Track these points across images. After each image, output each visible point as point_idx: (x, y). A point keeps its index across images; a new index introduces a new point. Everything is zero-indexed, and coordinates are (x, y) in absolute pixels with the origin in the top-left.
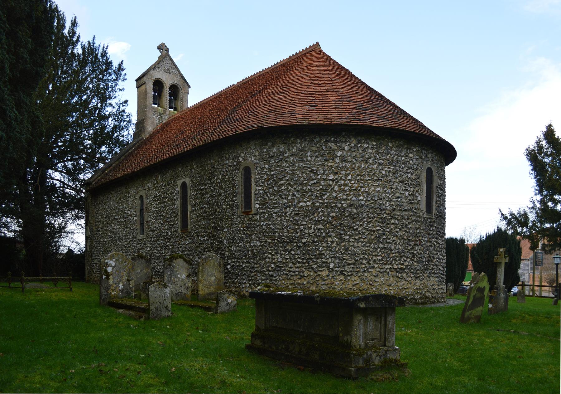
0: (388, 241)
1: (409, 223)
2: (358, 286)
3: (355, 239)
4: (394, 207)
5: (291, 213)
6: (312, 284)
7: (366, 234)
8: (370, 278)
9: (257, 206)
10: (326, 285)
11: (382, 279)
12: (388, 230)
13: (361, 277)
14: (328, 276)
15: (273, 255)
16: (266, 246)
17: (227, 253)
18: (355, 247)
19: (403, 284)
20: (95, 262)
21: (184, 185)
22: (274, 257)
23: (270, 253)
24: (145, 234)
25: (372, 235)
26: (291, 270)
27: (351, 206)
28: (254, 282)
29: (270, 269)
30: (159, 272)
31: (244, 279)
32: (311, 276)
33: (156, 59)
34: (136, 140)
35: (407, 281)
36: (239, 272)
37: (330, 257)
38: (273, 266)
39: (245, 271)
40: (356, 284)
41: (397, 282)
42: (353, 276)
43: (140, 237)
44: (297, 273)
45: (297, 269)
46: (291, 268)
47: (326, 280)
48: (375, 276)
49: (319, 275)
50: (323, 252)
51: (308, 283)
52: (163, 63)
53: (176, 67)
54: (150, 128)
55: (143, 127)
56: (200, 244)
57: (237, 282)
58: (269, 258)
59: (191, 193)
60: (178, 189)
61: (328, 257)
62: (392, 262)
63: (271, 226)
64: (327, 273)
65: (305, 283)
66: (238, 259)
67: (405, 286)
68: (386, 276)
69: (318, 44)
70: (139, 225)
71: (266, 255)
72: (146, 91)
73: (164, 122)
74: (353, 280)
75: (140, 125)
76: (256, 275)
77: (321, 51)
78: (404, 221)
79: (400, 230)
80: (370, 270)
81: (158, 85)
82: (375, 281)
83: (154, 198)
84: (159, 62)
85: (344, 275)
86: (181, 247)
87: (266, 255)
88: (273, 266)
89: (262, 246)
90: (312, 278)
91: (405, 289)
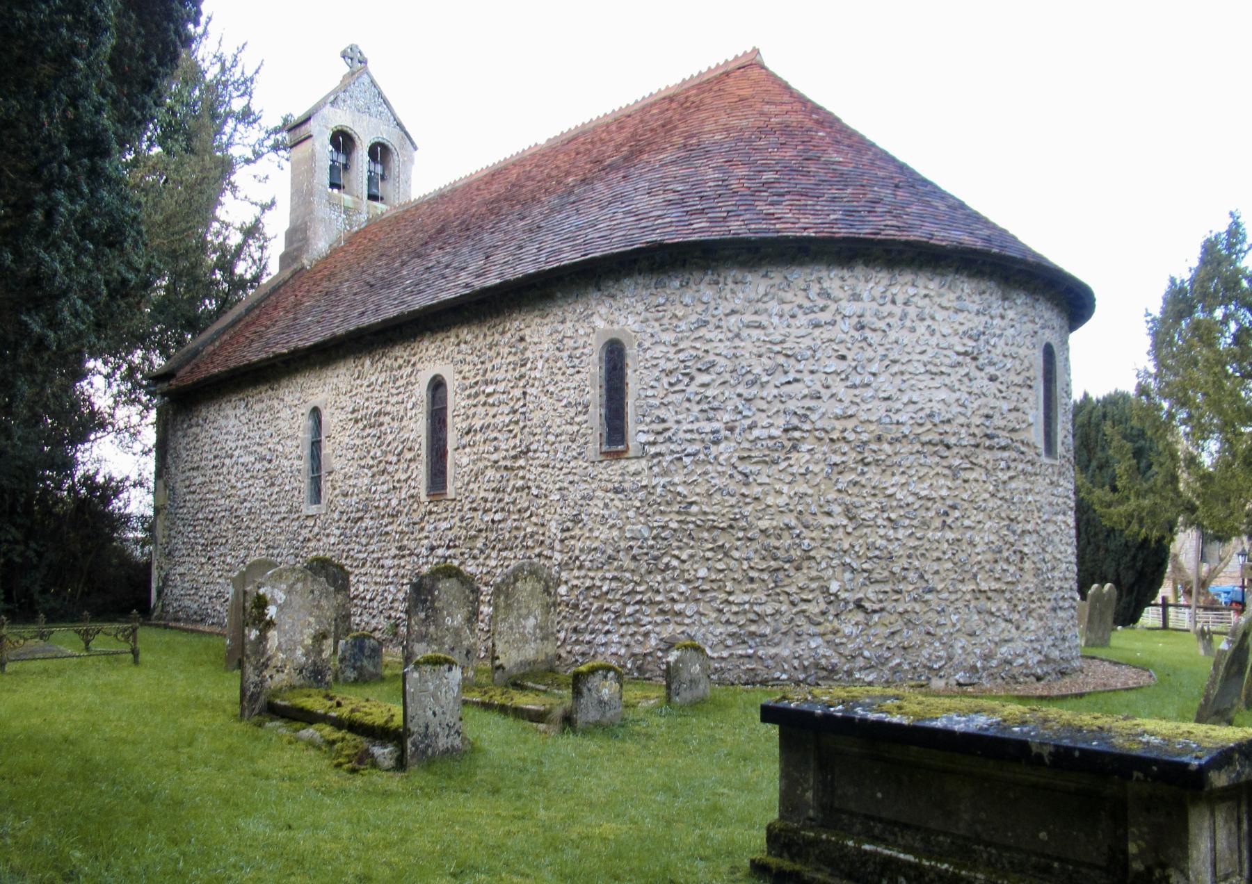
0: (967, 523)
1: (1011, 478)
2: (898, 638)
3: (889, 519)
4: (978, 440)
5: (730, 458)
6: (785, 634)
7: (916, 506)
8: (926, 617)
9: (643, 438)
10: (823, 635)
11: (954, 618)
12: (965, 496)
13: (907, 616)
14: (823, 613)
15: (684, 562)
16: (665, 539)
17: (558, 556)
18: (889, 540)
19: (1003, 631)
20: (181, 570)
21: (437, 385)
22: (686, 566)
23: (677, 558)
24: (324, 501)
25: (928, 509)
26: (731, 598)
27: (879, 439)
28: (633, 629)
29: (675, 596)
30: (363, 599)
31: (605, 623)
32: (781, 614)
33: (335, 82)
34: (288, 273)
35: (1010, 621)
36: (591, 604)
37: (829, 566)
38: (683, 588)
39: (610, 601)
40: (893, 633)
41: (986, 623)
42: (884, 614)
43: (313, 510)
44: (747, 606)
45: (746, 598)
46: (730, 593)
47: (819, 624)
48: (939, 613)
49: (804, 611)
50: (812, 553)
51: (775, 631)
52: (355, 89)
53: (385, 102)
54: (321, 244)
55: (305, 240)
56: (480, 531)
57: (586, 629)
58: (675, 568)
59: (455, 401)
60: (421, 391)
61: (824, 565)
62: (975, 576)
63: (679, 489)
64: (823, 606)
65: (768, 631)
66: (589, 570)
67: (1006, 636)
68: (964, 610)
69: (756, 51)
70: (308, 481)
71: (665, 560)
72: (313, 155)
73: (356, 229)
74: (887, 622)
75: (297, 236)
76: (637, 611)
77: (763, 67)
78: (1000, 474)
79: (993, 495)
80: (928, 597)
81: (343, 141)
82: (938, 625)
83: (353, 412)
84: (345, 86)
85: (865, 610)
86: (427, 537)
87: (665, 560)
88: (683, 588)
89: (654, 538)
90: (785, 619)
91: (1006, 641)
